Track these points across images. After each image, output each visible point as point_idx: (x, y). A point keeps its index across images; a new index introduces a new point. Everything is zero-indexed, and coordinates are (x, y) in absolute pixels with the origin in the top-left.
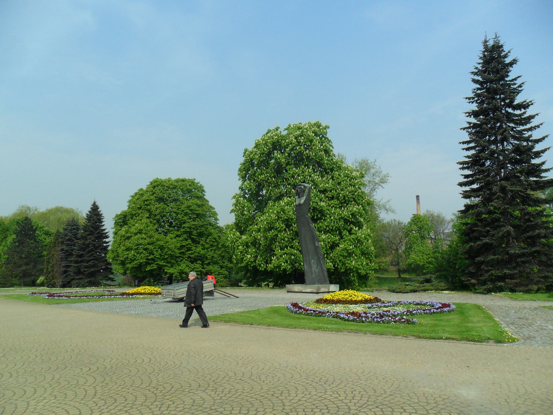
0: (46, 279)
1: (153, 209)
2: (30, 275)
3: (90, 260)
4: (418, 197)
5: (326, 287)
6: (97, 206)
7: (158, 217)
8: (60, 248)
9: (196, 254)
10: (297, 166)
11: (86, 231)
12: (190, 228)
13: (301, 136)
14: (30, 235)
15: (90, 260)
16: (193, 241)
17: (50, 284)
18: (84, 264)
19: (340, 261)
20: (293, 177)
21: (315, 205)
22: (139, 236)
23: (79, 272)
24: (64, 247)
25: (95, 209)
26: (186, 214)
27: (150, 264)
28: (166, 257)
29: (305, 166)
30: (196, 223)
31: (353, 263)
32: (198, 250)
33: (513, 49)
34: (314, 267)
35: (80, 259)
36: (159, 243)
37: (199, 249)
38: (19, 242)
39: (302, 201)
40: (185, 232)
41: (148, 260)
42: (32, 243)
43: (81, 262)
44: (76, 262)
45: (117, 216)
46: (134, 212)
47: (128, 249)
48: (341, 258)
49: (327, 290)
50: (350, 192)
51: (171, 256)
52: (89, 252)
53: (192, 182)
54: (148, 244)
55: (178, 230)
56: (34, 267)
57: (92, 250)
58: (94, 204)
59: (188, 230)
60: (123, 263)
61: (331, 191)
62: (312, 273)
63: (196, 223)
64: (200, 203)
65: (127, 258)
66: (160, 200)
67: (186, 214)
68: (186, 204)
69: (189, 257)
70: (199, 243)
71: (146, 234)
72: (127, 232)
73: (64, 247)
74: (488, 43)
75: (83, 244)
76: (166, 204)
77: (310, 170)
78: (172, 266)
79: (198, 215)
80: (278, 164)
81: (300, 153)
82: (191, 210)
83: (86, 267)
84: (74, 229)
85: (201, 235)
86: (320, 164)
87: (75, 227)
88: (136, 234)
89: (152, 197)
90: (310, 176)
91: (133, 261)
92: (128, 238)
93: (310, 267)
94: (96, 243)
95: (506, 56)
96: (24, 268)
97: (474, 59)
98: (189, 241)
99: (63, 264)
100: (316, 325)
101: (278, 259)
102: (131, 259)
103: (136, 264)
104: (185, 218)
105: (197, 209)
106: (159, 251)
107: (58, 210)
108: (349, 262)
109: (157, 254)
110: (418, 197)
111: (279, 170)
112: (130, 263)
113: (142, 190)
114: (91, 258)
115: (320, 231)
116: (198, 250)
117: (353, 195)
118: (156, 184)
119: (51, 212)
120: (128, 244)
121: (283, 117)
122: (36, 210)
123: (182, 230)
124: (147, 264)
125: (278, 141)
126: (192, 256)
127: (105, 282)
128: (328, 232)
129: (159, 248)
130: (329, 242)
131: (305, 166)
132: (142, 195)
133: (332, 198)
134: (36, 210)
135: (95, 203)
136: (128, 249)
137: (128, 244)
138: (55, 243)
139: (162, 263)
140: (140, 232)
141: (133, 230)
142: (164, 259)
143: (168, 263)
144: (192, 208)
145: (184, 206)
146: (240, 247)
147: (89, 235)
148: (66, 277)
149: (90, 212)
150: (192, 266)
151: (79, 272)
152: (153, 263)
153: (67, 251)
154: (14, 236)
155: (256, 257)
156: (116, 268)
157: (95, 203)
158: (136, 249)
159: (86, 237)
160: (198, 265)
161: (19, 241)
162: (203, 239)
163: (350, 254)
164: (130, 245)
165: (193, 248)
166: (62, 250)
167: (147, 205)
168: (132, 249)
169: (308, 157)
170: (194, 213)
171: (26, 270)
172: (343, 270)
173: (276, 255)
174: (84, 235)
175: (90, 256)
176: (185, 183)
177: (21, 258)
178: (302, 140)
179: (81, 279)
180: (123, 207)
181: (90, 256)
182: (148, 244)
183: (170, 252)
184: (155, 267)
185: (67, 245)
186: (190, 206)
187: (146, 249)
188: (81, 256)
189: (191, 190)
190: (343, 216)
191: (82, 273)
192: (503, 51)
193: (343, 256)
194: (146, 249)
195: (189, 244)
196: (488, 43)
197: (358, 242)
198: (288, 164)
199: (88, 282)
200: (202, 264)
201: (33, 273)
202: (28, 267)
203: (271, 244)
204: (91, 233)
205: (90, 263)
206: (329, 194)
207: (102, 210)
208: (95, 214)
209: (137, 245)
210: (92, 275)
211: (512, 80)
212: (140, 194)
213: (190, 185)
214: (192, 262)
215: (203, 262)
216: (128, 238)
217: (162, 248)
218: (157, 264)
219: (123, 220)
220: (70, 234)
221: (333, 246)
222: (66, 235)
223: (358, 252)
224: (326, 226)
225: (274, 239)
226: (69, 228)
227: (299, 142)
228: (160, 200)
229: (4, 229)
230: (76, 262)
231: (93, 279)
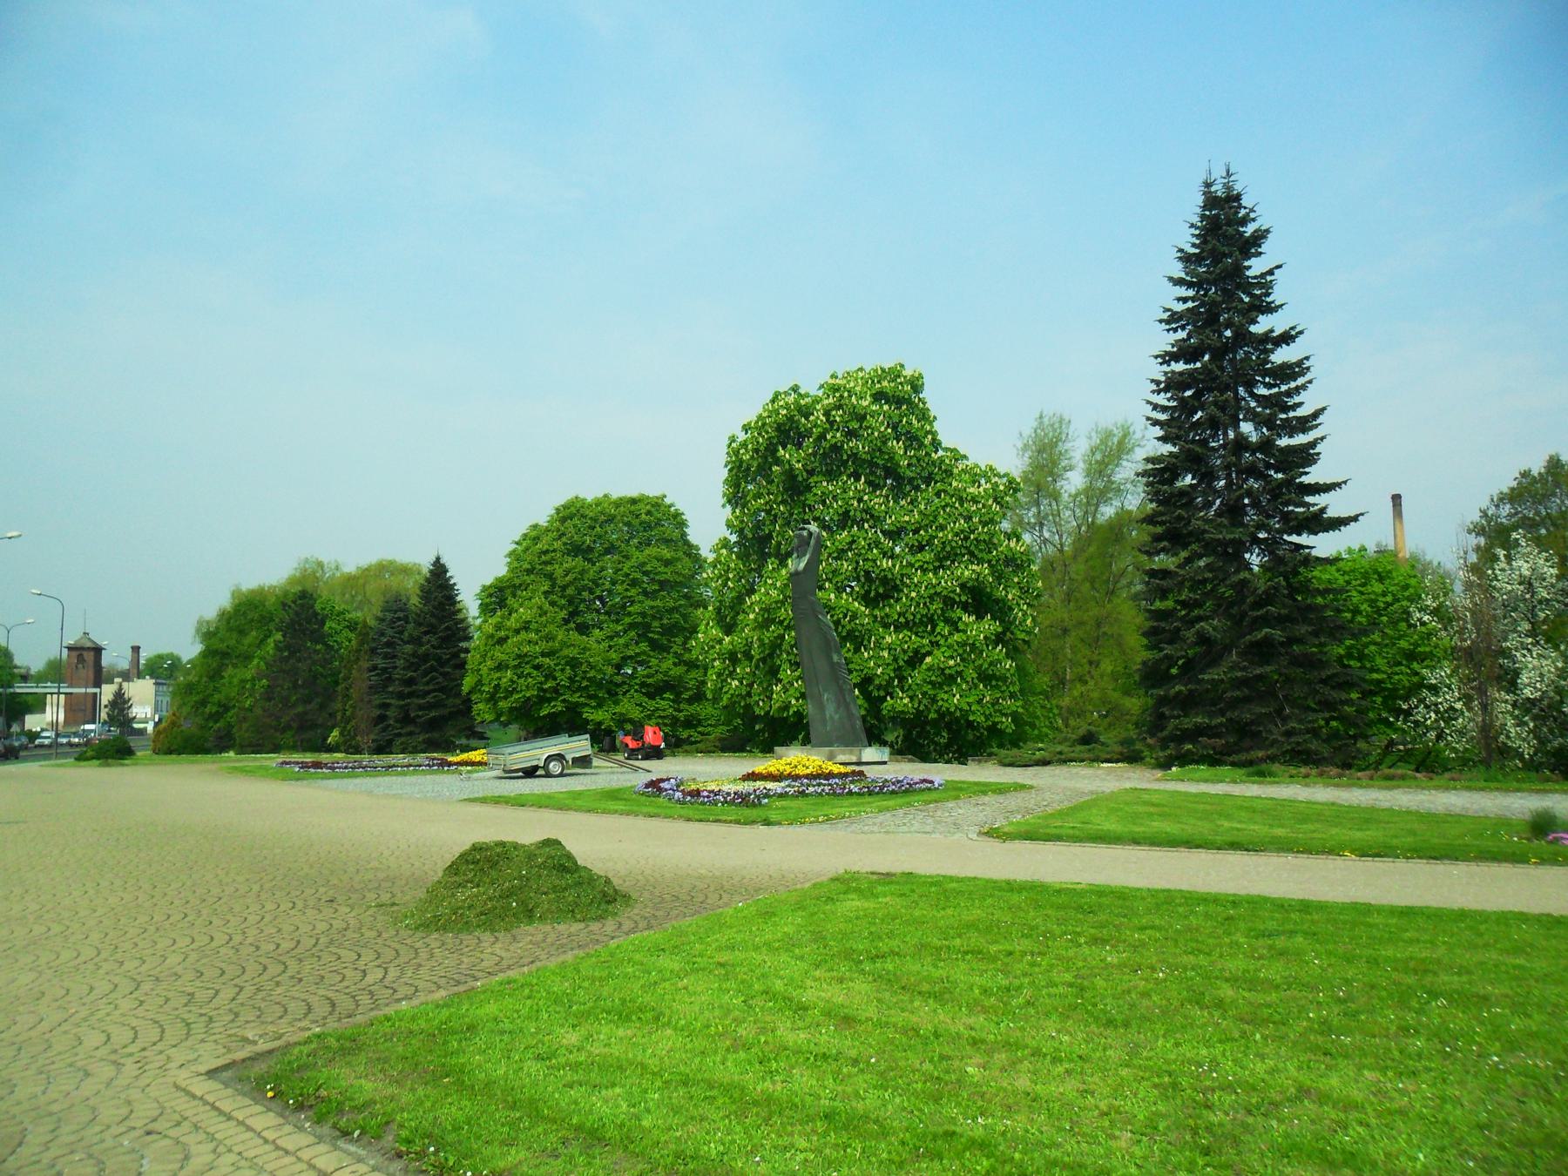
0: (341, 734)
1: (559, 572)
2: (314, 726)
3: (429, 693)
4: (1396, 499)
5: (851, 753)
6: (443, 566)
7: (570, 591)
8: (367, 665)
9: (660, 676)
10: (831, 475)
11: (420, 625)
12: (643, 615)
13: (839, 407)
14: (312, 632)
15: (429, 693)
16: (655, 645)
17: (350, 746)
18: (416, 701)
19: (924, 694)
20: (824, 503)
21: (869, 565)
22: (523, 635)
23: (406, 719)
24: (379, 661)
25: (439, 570)
26: (634, 583)
27: (549, 700)
28: (585, 683)
29: (849, 477)
30: (658, 603)
31: (955, 699)
32: (664, 666)
33: (1264, 205)
34: (830, 709)
35: (407, 690)
36: (566, 652)
37: (668, 664)
38: (290, 650)
39: (802, 566)
40: (632, 626)
41: (545, 691)
42: (317, 652)
43: (411, 695)
44: (401, 696)
45: (484, 589)
46: (517, 582)
47: (500, 667)
48: (927, 688)
49: (854, 759)
50: (957, 535)
51: (599, 685)
52: (426, 673)
53: (657, 504)
54: (543, 655)
55: (617, 621)
56: (322, 707)
57: (433, 669)
58: (1268, 231)
59: (639, 619)
60: (493, 699)
61: (916, 532)
62: (824, 721)
63: (658, 603)
64: (668, 556)
65: (498, 686)
66: (576, 550)
67: (634, 583)
68: (638, 556)
69: (643, 685)
70: (666, 649)
71: (537, 631)
72: (498, 627)
73: (379, 661)
74: (1213, 189)
75: (414, 655)
76: (589, 560)
77: (861, 485)
78: (600, 706)
79: (663, 584)
80: (790, 475)
81: (836, 448)
82: (646, 573)
83: (421, 708)
84: (399, 619)
85: (670, 631)
86: (891, 471)
87: (401, 615)
88: (517, 632)
89: (557, 545)
90: (860, 500)
91: (511, 693)
92: (502, 641)
93: (821, 708)
94: (445, 654)
95: (1245, 221)
96: (300, 709)
97: (1179, 228)
98: (644, 646)
99: (377, 699)
100: (651, 810)
101: (786, 690)
102: (506, 690)
103: (516, 701)
104: (633, 592)
105: (662, 569)
106: (568, 670)
107: (383, 568)
108: (945, 697)
109: (563, 678)
110: (1396, 499)
111: (795, 488)
112: (505, 698)
113: (535, 526)
114: (431, 687)
115: (886, 626)
116: (664, 666)
117: (966, 538)
118: (570, 513)
119: (368, 574)
120: (499, 654)
121: (815, 361)
122: (337, 568)
123: (627, 620)
124: (542, 700)
125: (790, 419)
126: (650, 681)
127: (464, 741)
128: (906, 625)
129: (567, 664)
130: (905, 652)
131: (849, 477)
132: (536, 539)
133: (921, 548)
134: (337, 568)
135: (438, 559)
136: (500, 667)
137: (499, 654)
138: (358, 651)
139: (575, 698)
140: (526, 627)
141: (512, 622)
142: (580, 689)
143: (590, 697)
144: (648, 568)
145: (629, 564)
146: (717, 663)
147: (426, 633)
148: (384, 730)
149: (428, 580)
150: (651, 705)
151: (406, 719)
152: (555, 699)
153: (385, 670)
154: (279, 636)
155: (751, 685)
156: (482, 711)
157: (438, 559)
158: (515, 667)
159: (419, 638)
160: (664, 704)
161: (288, 647)
162: (679, 640)
163: (950, 679)
164: (504, 657)
165: (654, 662)
166: (375, 668)
167: (546, 563)
168: (507, 667)
169: (854, 456)
170: (653, 580)
171: (305, 713)
172: (933, 716)
173: (780, 681)
174: (416, 634)
175: (428, 683)
176: (641, 505)
177: (295, 686)
178: (837, 415)
179: (410, 734)
180: (497, 568)
181: (428, 683)
182: (543, 655)
183: (592, 674)
184: (560, 707)
185: (386, 656)
186: (644, 564)
187: (537, 667)
188: (410, 682)
189: (652, 522)
190: (939, 589)
191: (412, 721)
192: (1240, 206)
193: (931, 683)
194: (537, 667)
195: (644, 653)
196: (1213, 189)
197: (971, 651)
198: (811, 473)
199: (424, 741)
200: (677, 701)
201: (320, 721)
202: (309, 707)
203: (771, 655)
204: (432, 630)
205: (429, 699)
206: (910, 538)
207: (456, 574)
208: (439, 581)
209: (519, 656)
210: (433, 725)
211: (1263, 275)
212: (534, 536)
213: (649, 513)
214: (651, 696)
215: (678, 694)
216: (502, 641)
217: (573, 663)
218: (564, 701)
219: (498, 597)
220: (389, 632)
221: (916, 659)
222: (383, 634)
223: (971, 673)
224: (900, 615)
225: (777, 644)
226: (389, 616)
227: (832, 423)
228: (576, 550)
229: (263, 617)
230: (401, 696)
231: (436, 735)
